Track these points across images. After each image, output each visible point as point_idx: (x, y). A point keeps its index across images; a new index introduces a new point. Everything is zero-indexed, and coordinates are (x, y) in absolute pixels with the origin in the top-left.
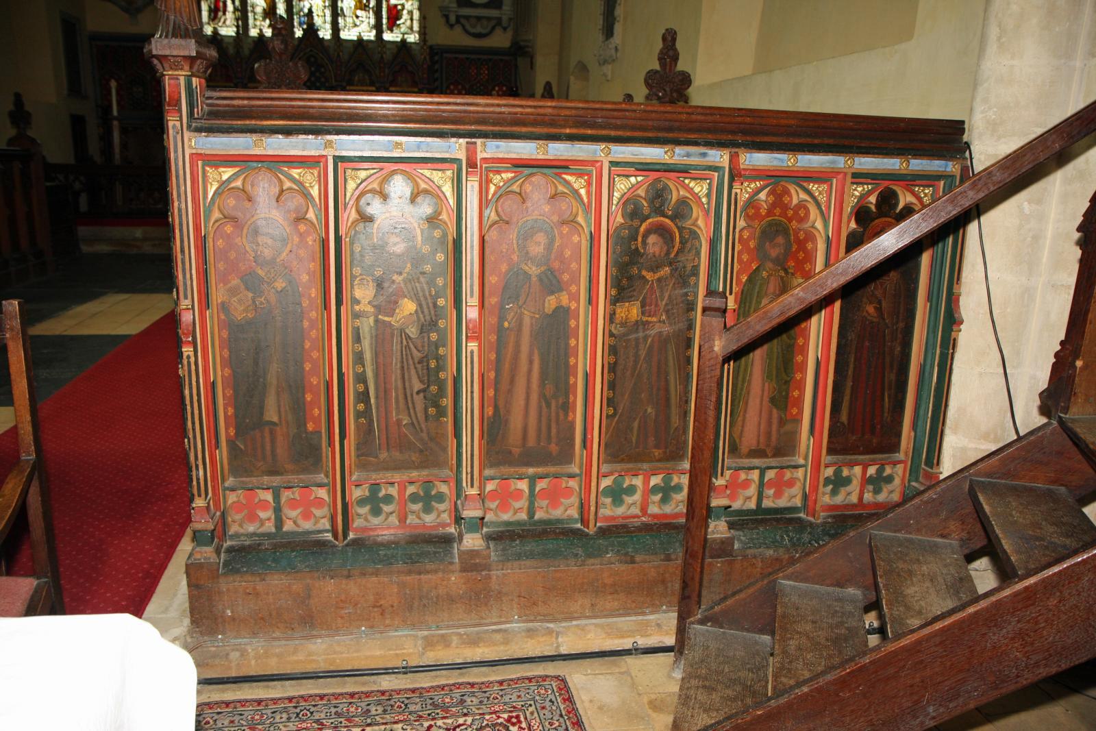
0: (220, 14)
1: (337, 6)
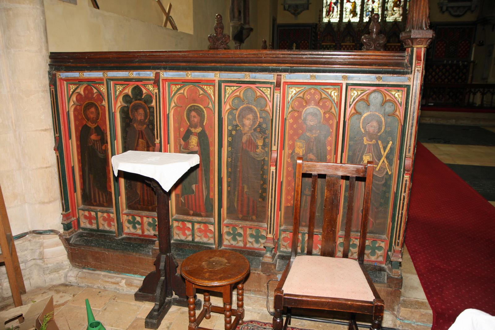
0: (331, 13)
1: (385, 6)
